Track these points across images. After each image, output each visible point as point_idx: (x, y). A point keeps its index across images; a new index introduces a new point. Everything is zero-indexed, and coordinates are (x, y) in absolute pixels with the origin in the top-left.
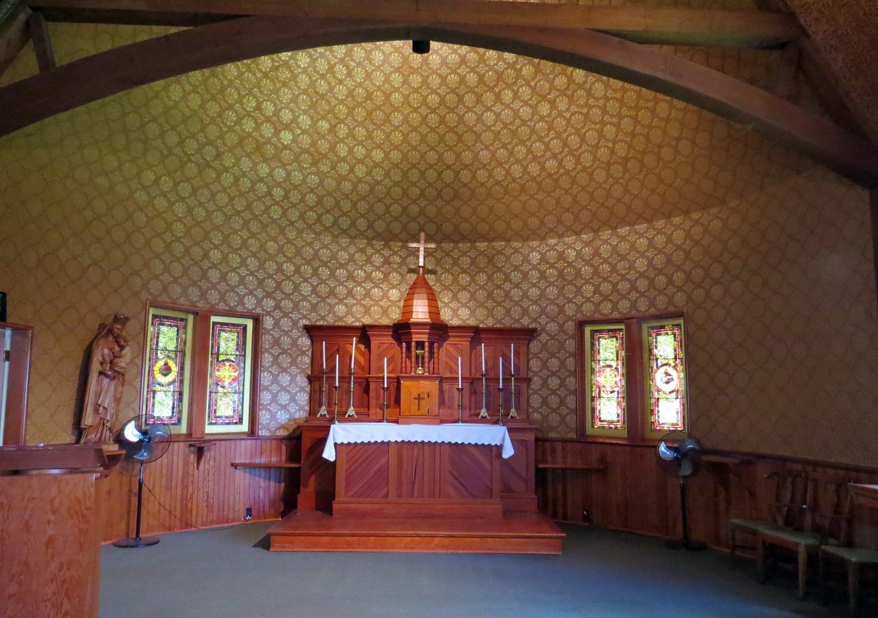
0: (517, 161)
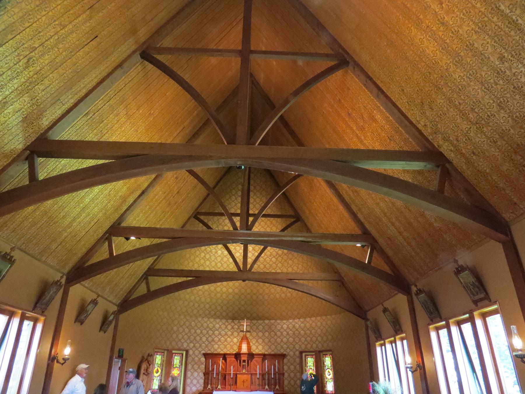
0: (278, 293)
